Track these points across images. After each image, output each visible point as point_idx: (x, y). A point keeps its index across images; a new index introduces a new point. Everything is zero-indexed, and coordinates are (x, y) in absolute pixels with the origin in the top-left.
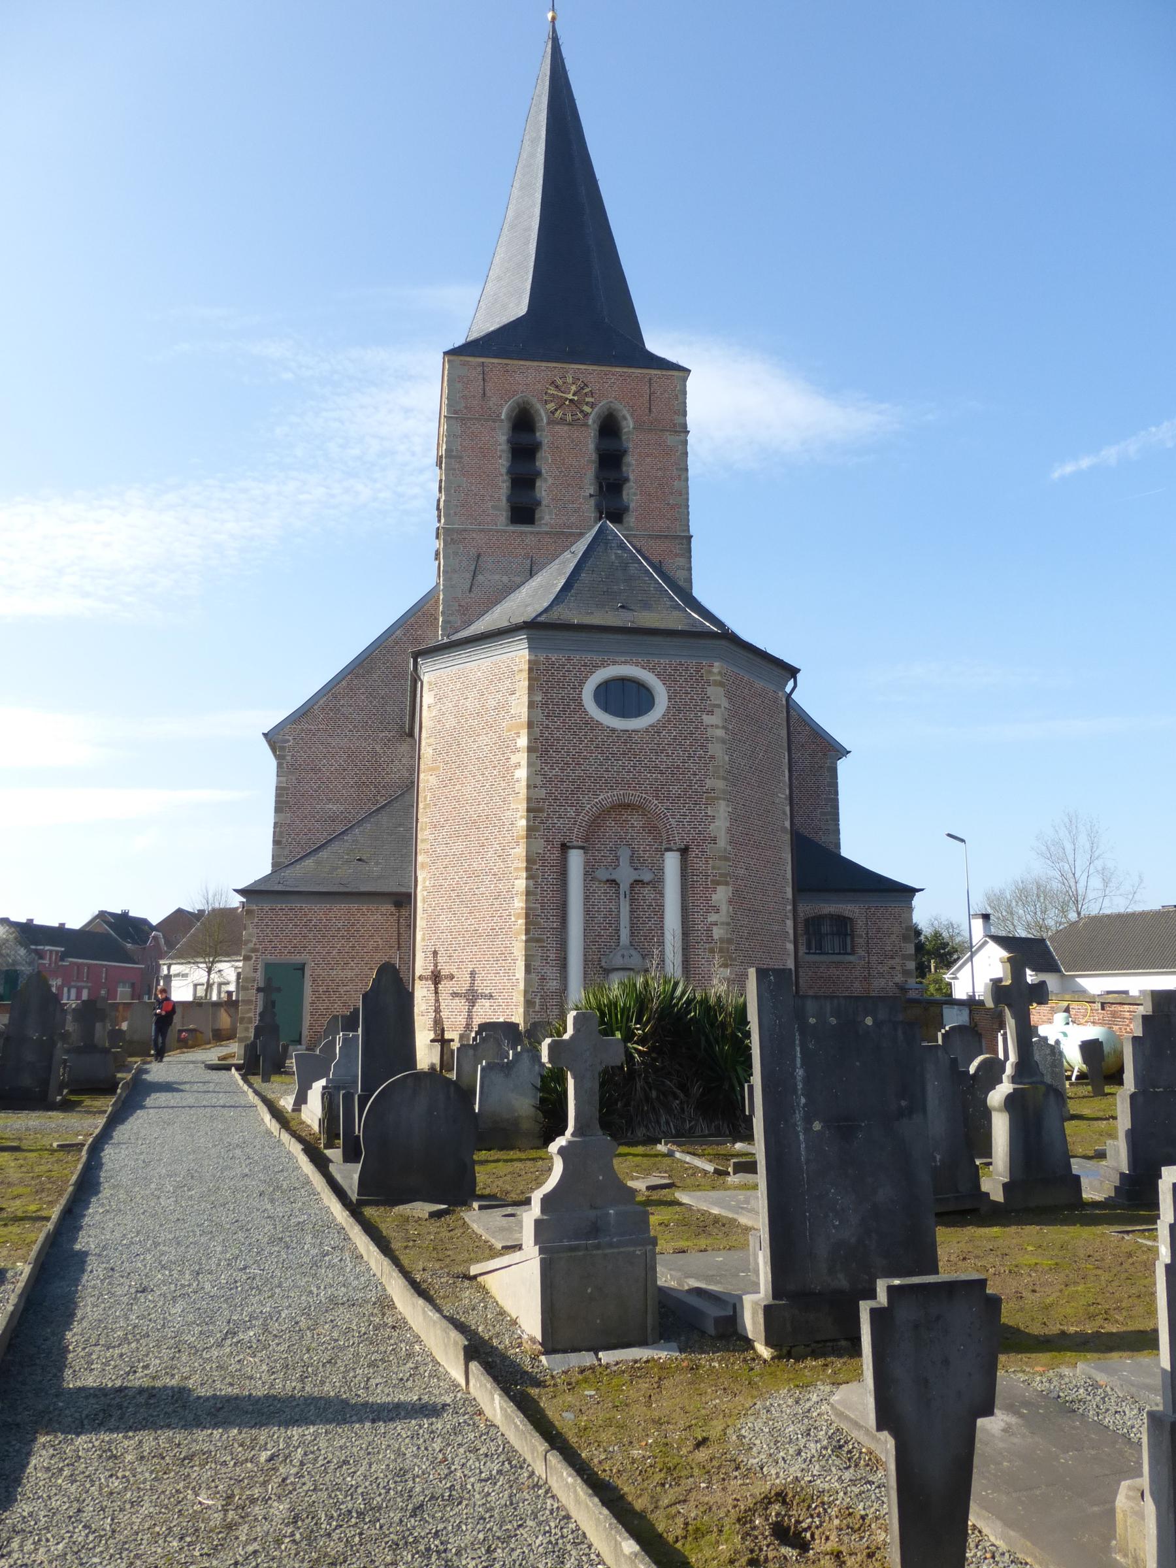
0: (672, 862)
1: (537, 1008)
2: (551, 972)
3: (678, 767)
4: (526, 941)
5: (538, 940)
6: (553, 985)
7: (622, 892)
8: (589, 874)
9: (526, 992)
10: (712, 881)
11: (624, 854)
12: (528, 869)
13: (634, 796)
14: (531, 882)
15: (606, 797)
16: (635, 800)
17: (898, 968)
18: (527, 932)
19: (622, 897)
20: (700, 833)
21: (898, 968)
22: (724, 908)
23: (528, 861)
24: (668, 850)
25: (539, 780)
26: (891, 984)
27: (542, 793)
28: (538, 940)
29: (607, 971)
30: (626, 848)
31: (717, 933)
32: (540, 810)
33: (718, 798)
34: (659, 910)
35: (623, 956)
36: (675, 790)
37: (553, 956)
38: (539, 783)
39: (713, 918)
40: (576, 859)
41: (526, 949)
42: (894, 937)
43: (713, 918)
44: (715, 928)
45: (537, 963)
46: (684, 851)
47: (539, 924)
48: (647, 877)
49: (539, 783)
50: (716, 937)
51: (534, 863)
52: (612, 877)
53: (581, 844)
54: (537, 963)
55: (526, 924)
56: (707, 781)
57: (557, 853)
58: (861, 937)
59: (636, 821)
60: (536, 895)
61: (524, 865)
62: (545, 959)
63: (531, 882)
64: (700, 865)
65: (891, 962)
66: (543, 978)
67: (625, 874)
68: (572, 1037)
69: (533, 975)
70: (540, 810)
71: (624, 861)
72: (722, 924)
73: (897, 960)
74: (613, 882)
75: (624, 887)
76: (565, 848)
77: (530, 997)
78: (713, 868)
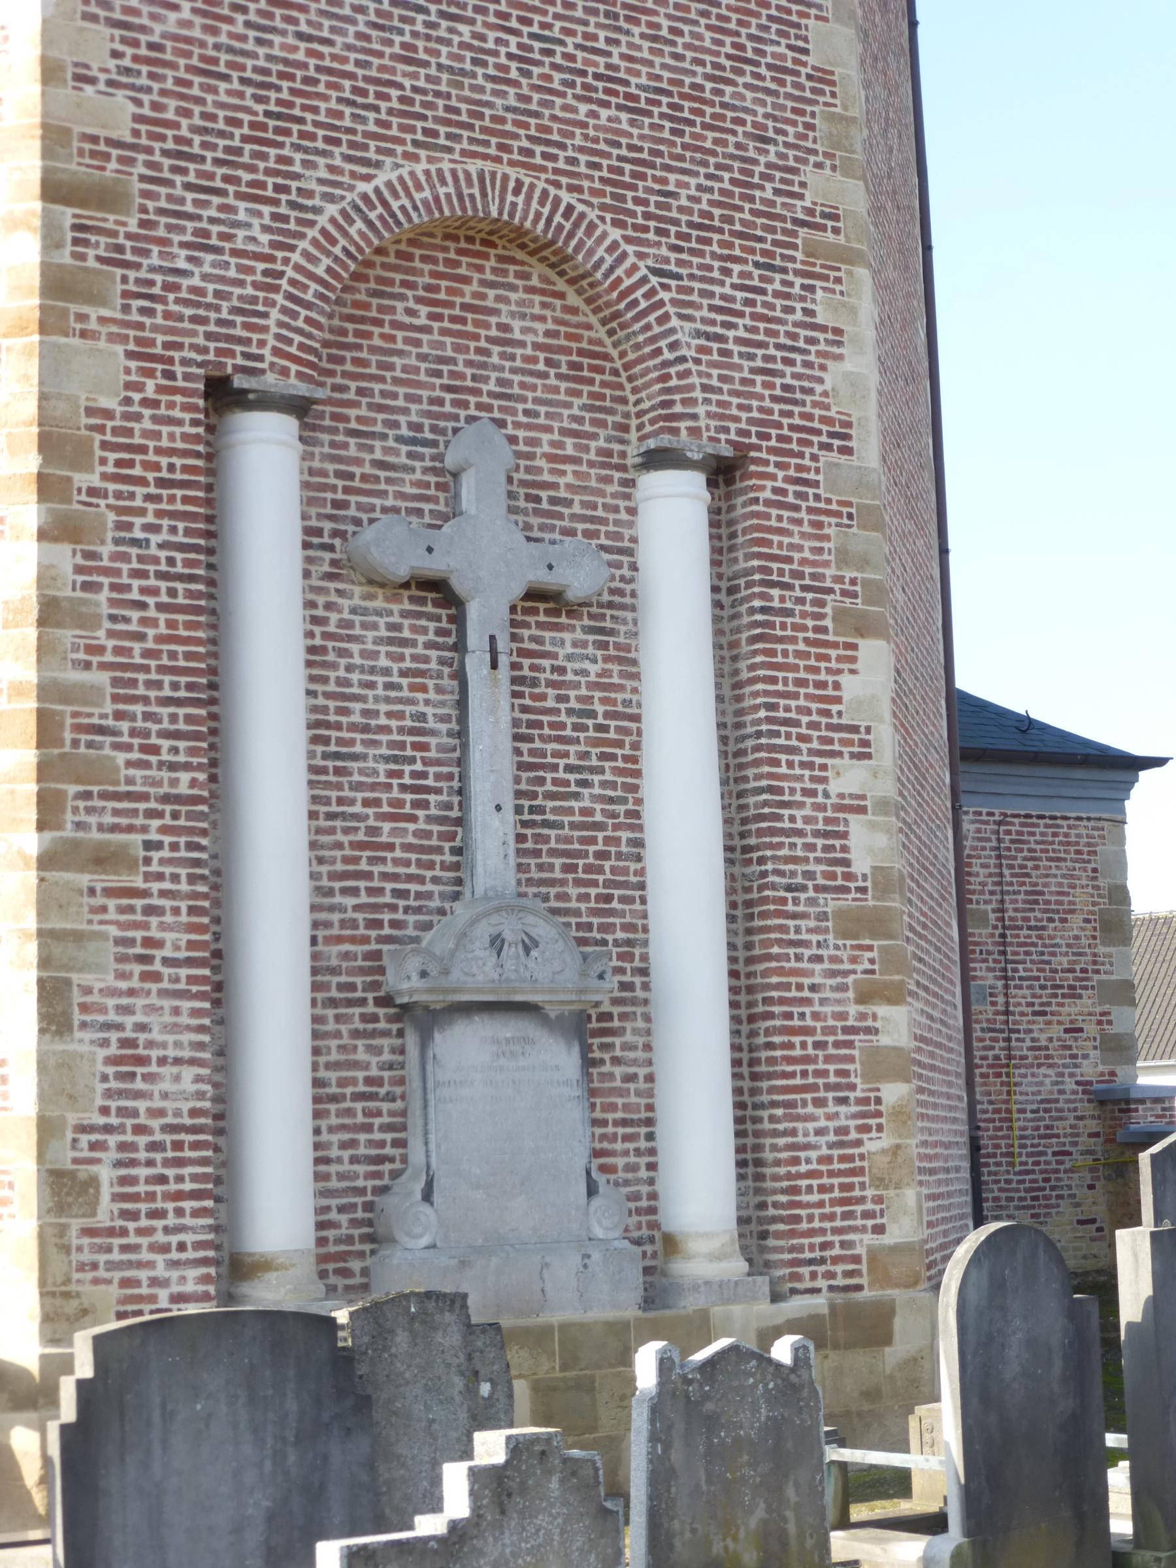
0: (672, 515)
1: (106, 1212)
2: (171, 1024)
3: (695, 94)
4: (46, 862)
5: (103, 859)
6: (180, 1089)
7: (476, 639)
8: (327, 543)
9: (47, 1129)
10: (839, 615)
11: (483, 464)
12: (48, 487)
13: (524, 197)
14: (65, 556)
15: (412, 179)
16: (530, 215)
17: (1091, 1029)
18: (48, 812)
19: (476, 664)
20: (787, 396)
21: (1091, 1029)
22: (885, 737)
23: (48, 443)
24: (658, 459)
25: (97, 46)
26: (1070, 1085)
27: (118, 115)
28: (103, 859)
29: (422, 1019)
30: (498, 437)
31: (869, 846)
32: (108, 198)
33: (851, 257)
34: (619, 738)
35: (497, 943)
36: (689, 191)
37: (175, 943)
38: (99, 60)
39: (848, 778)
40: (267, 458)
41: (46, 904)
42: (1076, 921)
43: (848, 778)
44: (855, 823)
45: (98, 977)
46: (723, 474)
47: (106, 772)
48: (581, 577)
49: (99, 60)
50: (861, 864)
51: (80, 458)
52: (434, 566)
53: (297, 387)
54: (98, 977)
55: (44, 770)
56: (808, 173)
57: (185, 421)
58: (983, 919)
59: (521, 313)
60: (88, 621)
61: (31, 462)
62: (141, 954)
63: (65, 556)
64: (795, 540)
65: (1070, 1010)
66: (130, 1059)
67: (491, 559)
68: (1155, 1305)
69: (82, 1042)
70: (108, 198)
71: (481, 493)
72: (883, 806)
73: (1088, 1002)
74: (438, 591)
75: (485, 615)
76: (222, 396)
77: (65, 1158)
78: (844, 557)
